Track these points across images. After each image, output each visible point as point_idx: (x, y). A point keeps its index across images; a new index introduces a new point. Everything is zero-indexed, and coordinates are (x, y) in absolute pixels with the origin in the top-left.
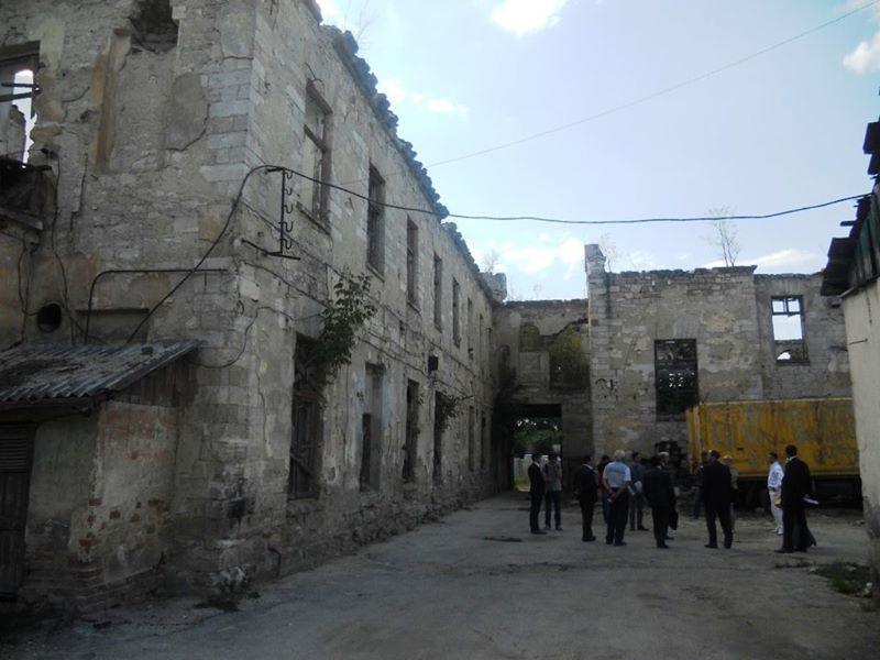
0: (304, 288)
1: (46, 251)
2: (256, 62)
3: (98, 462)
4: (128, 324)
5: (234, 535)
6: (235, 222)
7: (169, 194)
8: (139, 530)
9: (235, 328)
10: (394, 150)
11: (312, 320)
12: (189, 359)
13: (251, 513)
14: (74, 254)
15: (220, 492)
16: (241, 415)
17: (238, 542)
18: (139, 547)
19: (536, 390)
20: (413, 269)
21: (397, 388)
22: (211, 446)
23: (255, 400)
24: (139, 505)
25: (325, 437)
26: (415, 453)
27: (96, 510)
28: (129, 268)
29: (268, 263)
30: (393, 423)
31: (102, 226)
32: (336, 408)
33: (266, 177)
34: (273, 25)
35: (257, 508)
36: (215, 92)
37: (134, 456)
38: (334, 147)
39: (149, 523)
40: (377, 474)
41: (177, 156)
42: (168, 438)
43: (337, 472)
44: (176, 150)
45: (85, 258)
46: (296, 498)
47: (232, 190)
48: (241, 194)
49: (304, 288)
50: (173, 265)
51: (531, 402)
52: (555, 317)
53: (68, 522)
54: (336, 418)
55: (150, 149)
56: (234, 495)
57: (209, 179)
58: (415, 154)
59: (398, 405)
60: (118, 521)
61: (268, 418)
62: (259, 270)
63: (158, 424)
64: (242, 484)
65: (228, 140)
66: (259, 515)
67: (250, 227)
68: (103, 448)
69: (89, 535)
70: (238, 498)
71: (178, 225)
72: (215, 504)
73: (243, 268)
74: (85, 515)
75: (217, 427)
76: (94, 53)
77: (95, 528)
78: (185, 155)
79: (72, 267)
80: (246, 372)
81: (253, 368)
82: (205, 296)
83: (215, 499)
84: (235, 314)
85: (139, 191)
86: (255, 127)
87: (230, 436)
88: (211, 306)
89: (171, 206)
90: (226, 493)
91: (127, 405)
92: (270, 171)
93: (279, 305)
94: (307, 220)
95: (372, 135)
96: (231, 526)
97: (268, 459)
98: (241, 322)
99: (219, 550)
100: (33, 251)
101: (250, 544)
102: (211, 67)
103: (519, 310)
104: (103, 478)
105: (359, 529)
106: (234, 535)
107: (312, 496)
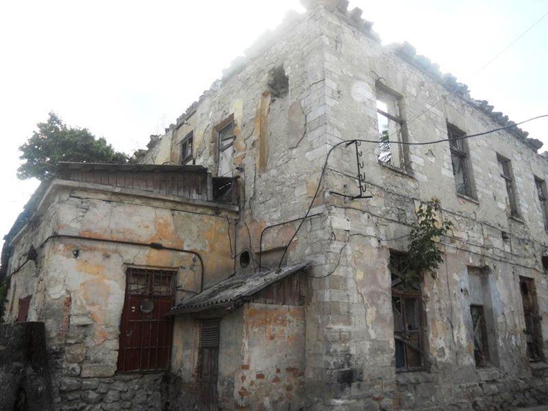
0: (394, 217)
1: (241, 223)
2: (327, 81)
3: (245, 341)
4: (276, 257)
5: (346, 397)
6: (324, 181)
7: (303, 177)
8: (280, 388)
9: (331, 250)
10: (471, 109)
11: (404, 239)
12: (305, 273)
13: (360, 380)
14: (253, 221)
15: (330, 364)
16: (343, 309)
17: (349, 402)
18: (281, 399)
20: (513, 191)
21: (507, 284)
22: (323, 331)
23: (355, 298)
24: (278, 371)
25: (430, 323)
26: (541, 337)
27: (245, 372)
28: (276, 223)
29: (356, 204)
30: (507, 311)
31: (263, 203)
32: (439, 301)
33: (348, 149)
34: (339, 55)
35: (365, 377)
36: (308, 107)
37: (272, 338)
38: (408, 119)
39: (287, 384)
40: (496, 353)
41: (294, 151)
42: (297, 326)
43: (447, 351)
44: (293, 148)
45: (257, 222)
46: (409, 371)
47: (322, 164)
48: (326, 163)
49: (394, 217)
50: (296, 217)
53: (233, 379)
54: (440, 309)
55: (284, 152)
56: (343, 366)
57: (310, 160)
58: (492, 107)
59: (510, 296)
60: (264, 381)
61: (369, 311)
62: (348, 210)
63: (289, 317)
64: (349, 358)
65: (317, 133)
66: (369, 382)
67: (337, 183)
68: (247, 332)
69: (243, 388)
70: (346, 368)
71: (298, 192)
72: (328, 372)
73: (334, 210)
74: (240, 375)
75: (325, 318)
76: (255, 109)
77: (246, 384)
78: (298, 148)
79: (252, 228)
80: (345, 280)
81: (351, 275)
82: (313, 233)
83: (328, 369)
84: (331, 241)
85: (279, 177)
86: (333, 120)
87: (334, 323)
88: (316, 238)
89: (293, 181)
90: (334, 364)
91: (263, 305)
92: (348, 144)
93: (370, 231)
94: (391, 172)
95: (446, 103)
96: (342, 389)
97: (371, 340)
98: (336, 246)
99: (333, 406)
100: (237, 224)
101: (361, 404)
102: (306, 93)
104: (249, 351)
105: (479, 399)
106: (347, 396)
107: (424, 370)
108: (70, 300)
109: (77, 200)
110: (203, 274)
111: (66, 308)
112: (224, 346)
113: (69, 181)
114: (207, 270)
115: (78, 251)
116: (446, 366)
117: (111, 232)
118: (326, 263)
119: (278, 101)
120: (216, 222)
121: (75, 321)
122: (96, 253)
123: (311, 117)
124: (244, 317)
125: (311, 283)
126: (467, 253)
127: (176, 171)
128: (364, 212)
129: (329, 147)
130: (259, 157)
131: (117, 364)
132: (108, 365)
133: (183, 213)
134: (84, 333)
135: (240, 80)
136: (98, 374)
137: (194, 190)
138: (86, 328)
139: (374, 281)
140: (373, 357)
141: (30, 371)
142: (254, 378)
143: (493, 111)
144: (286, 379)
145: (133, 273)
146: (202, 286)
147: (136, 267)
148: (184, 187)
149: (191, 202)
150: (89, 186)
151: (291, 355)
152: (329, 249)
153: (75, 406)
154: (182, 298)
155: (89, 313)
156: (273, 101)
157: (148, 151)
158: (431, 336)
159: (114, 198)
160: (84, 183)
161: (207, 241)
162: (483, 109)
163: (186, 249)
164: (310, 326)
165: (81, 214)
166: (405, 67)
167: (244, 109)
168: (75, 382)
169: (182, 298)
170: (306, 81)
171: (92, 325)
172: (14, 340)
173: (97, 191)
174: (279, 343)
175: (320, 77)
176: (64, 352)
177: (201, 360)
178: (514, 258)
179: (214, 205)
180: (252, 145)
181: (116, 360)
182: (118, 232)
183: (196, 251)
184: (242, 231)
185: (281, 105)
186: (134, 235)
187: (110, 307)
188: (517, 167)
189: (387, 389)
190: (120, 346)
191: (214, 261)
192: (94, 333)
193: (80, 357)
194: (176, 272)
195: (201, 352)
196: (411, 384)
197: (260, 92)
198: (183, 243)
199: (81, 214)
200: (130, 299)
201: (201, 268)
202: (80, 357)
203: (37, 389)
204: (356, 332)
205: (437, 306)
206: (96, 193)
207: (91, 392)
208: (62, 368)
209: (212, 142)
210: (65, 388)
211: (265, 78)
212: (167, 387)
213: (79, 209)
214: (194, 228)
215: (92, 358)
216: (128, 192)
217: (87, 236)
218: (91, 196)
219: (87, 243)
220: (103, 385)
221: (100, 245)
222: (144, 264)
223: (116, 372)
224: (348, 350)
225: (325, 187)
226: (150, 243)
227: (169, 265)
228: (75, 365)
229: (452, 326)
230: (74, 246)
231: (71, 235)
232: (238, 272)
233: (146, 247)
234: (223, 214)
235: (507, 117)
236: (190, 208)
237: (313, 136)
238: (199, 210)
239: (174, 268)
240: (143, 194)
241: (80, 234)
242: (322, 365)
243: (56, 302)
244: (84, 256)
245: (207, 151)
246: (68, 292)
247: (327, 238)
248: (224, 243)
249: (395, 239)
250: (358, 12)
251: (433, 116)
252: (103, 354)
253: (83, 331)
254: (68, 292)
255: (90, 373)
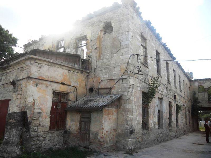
1: (90, 77)
4: (106, 91)
12: (120, 99)
14: (95, 77)
16: (131, 110)
19: (204, 103)
22: (125, 117)
24: (111, 130)
25: (150, 115)
26: (171, 120)
28: (106, 79)
29: (136, 76)
35: (135, 132)
36: (122, 40)
37: (110, 119)
41: (115, 54)
43: (153, 124)
44: (115, 53)
47: (127, 61)
48: (129, 61)
49: (143, 81)
50: (115, 78)
51: (203, 106)
52: (208, 83)
53: (98, 133)
54: (152, 111)
57: (122, 59)
60: (107, 133)
65: (125, 50)
67: (131, 68)
68: (104, 117)
69: (102, 136)
70: (131, 129)
72: (127, 130)
73: (131, 78)
74: (101, 131)
75: (126, 113)
76: (97, 35)
78: (116, 54)
79: (95, 80)
86: (131, 46)
89: (114, 65)
90: (129, 128)
93: (138, 85)
97: (137, 121)
98: (131, 90)
102: (121, 34)
103: (198, 82)
105: (159, 138)
108: (34, 103)
109: (37, 64)
110: (77, 95)
111: (33, 106)
112: (93, 121)
113: (35, 56)
114: (78, 93)
115: (37, 84)
116: (152, 128)
117: (49, 78)
118: (127, 95)
119: (107, 34)
120: (81, 76)
121: (36, 111)
122: (43, 85)
123: (123, 44)
124: (103, 112)
125: (121, 101)
126: (158, 93)
127: (70, 56)
128: (137, 79)
129: (130, 56)
130: (98, 53)
131: (49, 127)
132: (46, 127)
133: (71, 72)
134: (39, 116)
135: (90, 23)
136: (43, 131)
137: (76, 63)
138: (39, 114)
139: (139, 102)
140: (137, 126)
141: (24, 130)
142: (105, 132)
143: (167, 47)
144: (113, 133)
145: (55, 93)
146: (76, 99)
147: (56, 91)
148: (73, 62)
149: (75, 68)
150: (42, 59)
151: (114, 125)
152: (129, 90)
153: (36, 143)
154: (70, 104)
155: (41, 108)
156: (105, 34)
157: (38, 41)
158: (150, 119)
159: (49, 64)
160: (41, 58)
161: (78, 83)
162: (164, 46)
163: (72, 85)
164: (120, 115)
165: (39, 69)
166: (147, 29)
167: (91, 34)
168: (36, 133)
169: (70, 104)
170: (121, 30)
171: (41, 113)
172: (19, 118)
173: (44, 61)
174: (111, 121)
175: (127, 30)
176: (32, 123)
177: (80, 126)
178: (168, 95)
179: (82, 69)
180: (95, 49)
181: (49, 125)
182: (51, 77)
183: (75, 86)
184: (91, 80)
185: (108, 36)
186: (56, 79)
187: (48, 106)
188: (170, 65)
189: (140, 136)
190: (50, 120)
191: (81, 90)
192: (42, 116)
193: (37, 124)
194: (68, 94)
195: (80, 123)
196: (145, 134)
197: (99, 29)
198: (71, 83)
199: (39, 69)
200: (54, 103)
201: (76, 93)
202: (37, 124)
203: (27, 137)
204: (134, 118)
205: (151, 110)
206: (44, 61)
207: (41, 137)
208: (31, 129)
209: (75, 44)
210: (32, 136)
211: (102, 25)
212: (66, 135)
213: (38, 67)
214: (75, 78)
215: (41, 125)
216: (55, 62)
217: (40, 78)
218: (42, 62)
219: (41, 81)
220: (45, 135)
221: (45, 82)
222: (59, 90)
223: (49, 130)
224: (132, 124)
225: (128, 69)
226: (61, 82)
227: (66, 91)
228: (36, 127)
229: (154, 116)
230: (36, 82)
231: (34, 77)
232: (88, 95)
233: (60, 84)
234: (84, 73)
235: (169, 49)
236: (74, 70)
237: (123, 50)
238: (77, 71)
239: (68, 92)
240: (60, 63)
241: (38, 77)
242: (124, 128)
243: (30, 103)
244: (39, 86)
245: (72, 47)
246: (34, 100)
247: (128, 87)
248: (83, 84)
249: (144, 88)
250: (139, 8)
251: (153, 47)
252: (45, 123)
253: (39, 115)
254: (34, 100)
255: (41, 130)
